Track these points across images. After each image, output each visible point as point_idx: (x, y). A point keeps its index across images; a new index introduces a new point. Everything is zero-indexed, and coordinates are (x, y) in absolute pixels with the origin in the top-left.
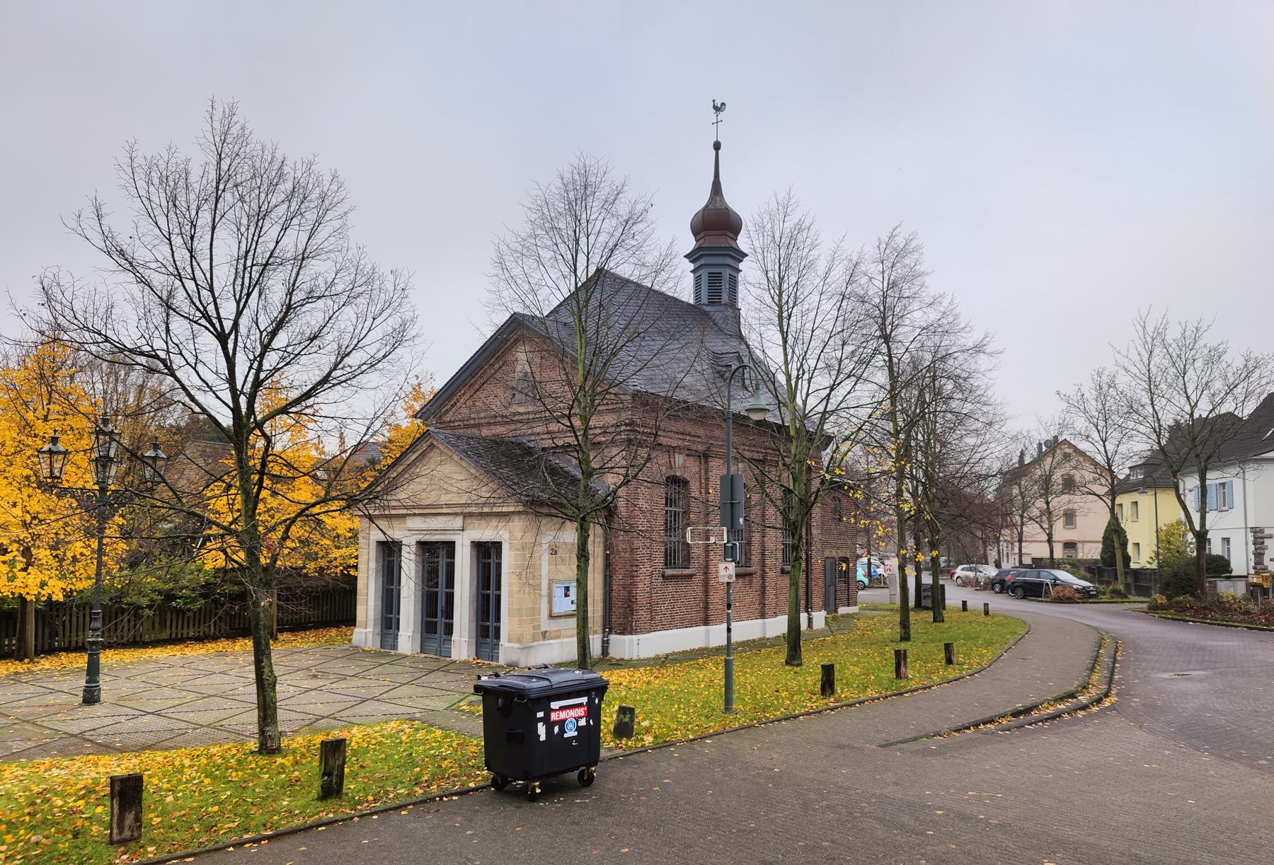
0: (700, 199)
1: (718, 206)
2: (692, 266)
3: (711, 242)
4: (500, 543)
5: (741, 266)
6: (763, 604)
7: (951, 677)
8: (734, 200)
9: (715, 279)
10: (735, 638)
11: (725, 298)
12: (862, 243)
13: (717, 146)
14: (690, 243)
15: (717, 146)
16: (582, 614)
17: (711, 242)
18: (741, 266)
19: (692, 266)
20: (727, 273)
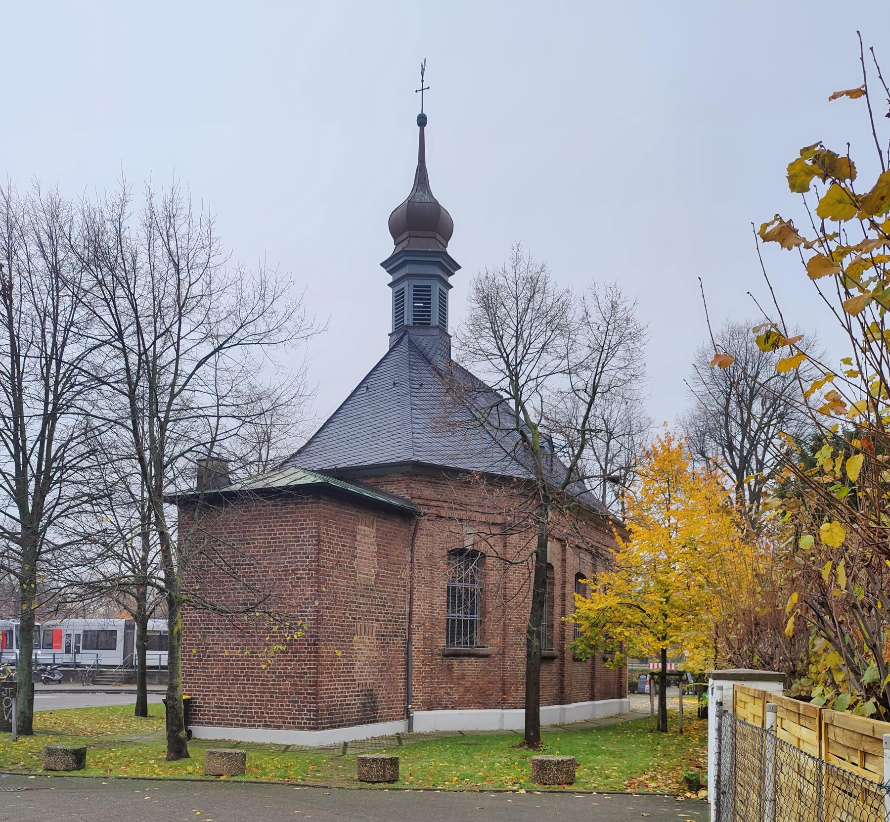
0: (400, 192)
1: (426, 198)
2: (390, 279)
3: (418, 245)
4: (137, 714)
5: (451, 280)
6: (592, 688)
7: (415, 637)
8: (442, 192)
9: (422, 294)
10: (418, 728)
11: (435, 321)
12: (561, 288)
13: (422, 121)
14: (387, 247)
15: (422, 121)
16: (447, 637)
17: (418, 245)
18: (451, 280)
19: (390, 279)
20: (436, 286)
